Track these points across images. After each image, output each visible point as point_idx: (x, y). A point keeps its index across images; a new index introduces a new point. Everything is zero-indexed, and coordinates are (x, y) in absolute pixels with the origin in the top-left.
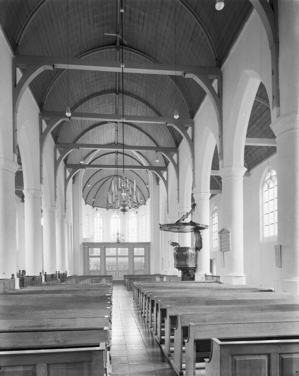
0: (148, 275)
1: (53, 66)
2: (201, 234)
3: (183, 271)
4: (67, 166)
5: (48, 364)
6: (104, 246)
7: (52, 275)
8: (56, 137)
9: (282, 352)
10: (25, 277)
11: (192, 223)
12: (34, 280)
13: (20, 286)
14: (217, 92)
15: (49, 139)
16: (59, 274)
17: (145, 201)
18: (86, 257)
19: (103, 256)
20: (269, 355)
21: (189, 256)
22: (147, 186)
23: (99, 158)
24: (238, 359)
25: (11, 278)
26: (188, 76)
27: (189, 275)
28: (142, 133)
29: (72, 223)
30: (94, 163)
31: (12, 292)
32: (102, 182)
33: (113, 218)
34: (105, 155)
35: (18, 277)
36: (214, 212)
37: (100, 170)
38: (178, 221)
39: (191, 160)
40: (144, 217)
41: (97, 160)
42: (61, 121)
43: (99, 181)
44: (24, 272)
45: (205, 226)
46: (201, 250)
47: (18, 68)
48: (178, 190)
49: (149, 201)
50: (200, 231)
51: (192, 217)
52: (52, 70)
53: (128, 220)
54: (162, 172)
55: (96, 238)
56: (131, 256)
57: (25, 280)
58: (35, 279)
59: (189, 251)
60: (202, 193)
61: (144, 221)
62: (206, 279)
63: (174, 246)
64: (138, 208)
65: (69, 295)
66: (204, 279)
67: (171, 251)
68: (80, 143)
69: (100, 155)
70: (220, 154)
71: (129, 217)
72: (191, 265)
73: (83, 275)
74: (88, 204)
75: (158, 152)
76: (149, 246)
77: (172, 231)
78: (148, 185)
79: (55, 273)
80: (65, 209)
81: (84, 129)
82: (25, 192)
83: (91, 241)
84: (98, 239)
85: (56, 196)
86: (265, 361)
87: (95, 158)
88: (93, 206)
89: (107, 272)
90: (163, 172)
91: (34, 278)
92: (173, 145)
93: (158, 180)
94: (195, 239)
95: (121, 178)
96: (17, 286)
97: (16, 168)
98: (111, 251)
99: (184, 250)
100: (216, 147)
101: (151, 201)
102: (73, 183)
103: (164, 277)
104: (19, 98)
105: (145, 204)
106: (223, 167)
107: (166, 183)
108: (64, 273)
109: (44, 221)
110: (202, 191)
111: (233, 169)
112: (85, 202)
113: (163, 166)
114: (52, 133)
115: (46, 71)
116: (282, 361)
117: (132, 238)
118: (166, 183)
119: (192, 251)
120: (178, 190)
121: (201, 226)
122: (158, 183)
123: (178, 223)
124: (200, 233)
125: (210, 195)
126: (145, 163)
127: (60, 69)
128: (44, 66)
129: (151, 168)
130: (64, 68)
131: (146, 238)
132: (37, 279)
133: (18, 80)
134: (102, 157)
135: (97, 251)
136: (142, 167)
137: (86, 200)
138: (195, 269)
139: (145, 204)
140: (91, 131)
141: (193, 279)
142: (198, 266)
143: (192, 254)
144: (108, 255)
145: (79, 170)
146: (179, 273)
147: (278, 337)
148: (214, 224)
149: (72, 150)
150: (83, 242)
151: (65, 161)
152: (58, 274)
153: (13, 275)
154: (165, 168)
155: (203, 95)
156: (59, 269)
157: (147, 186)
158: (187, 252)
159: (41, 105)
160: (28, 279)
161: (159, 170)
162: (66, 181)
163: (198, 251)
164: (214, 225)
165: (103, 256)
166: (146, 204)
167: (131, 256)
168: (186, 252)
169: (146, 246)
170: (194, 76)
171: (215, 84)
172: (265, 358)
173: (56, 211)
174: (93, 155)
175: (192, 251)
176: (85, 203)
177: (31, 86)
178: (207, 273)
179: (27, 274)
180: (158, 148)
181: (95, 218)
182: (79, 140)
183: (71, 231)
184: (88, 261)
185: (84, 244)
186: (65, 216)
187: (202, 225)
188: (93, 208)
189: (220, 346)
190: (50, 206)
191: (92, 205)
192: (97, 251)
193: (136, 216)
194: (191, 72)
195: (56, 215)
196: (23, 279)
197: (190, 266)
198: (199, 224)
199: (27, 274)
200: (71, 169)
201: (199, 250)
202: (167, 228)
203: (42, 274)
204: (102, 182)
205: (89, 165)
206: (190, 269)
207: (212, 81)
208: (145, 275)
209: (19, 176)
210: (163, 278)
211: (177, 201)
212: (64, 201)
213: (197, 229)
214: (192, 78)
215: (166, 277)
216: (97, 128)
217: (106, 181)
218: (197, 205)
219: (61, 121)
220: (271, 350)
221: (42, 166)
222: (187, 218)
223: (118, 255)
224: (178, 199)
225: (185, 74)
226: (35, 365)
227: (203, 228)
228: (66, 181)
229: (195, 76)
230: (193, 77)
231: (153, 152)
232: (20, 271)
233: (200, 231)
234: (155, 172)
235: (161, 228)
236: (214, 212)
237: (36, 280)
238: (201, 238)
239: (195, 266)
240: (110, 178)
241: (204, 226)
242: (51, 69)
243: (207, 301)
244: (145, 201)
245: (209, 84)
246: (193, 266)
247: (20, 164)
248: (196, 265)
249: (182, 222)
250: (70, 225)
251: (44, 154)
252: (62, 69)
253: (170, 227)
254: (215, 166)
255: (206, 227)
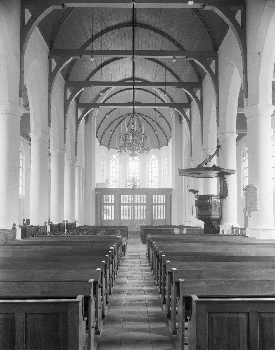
0: (170, 226)
1: (63, 5)
2: (226, 180)
3: (206, 223)
4: (79, 105)
5: (26, 314)
6: (118, 193)
7: (59, 225)
8: (66, 76)
9: (262, 310)
10: (29, 227)
11: (215, 168)
12: (38, 231)
13: (22, 237)
14: (240, 24)
15: (59, 78)
16: (67, 224)
17: (167, 141)
18: (99, 205)
19: (118, 204)
20: (248, 314)
21: (213, 205)
22: (156, 133)
23: (115, 95)
24: (214, 316)
25: (12, 228)
26: (207, 8)
27: (212, 227)
28: (162, 67)
29: (84, 167)
30: (109, 101)
31: (13, 243)
32: (119, 120)
33: (130, 160)
34: (122, 92)
35: (20, 226)
36: (245, 153)
37: (115, 108)
38: (200, 165)
39: (215, 97)
40: (166, 159)
41: (112, 97)
42: (71, 59)
43: (110, 125)
44: (28, 221)
45: (231, 170)
46: (226, 198)
47: (26, 8)
48: (202, 129)
49: (171, 141)
50: (225, 176)
51: (218, 161)
52: (61, 9)
53: (148, 162)
54: (184, 109)
55: (111, 184)
56: (150, 204)
57: (28, 231)
58: (40, 229)
59: (213, 199)
60: (227, 134)
61: (166, 163)
62: (232, 232)
63: (195, 194)
64: (160, 149)
65: (70, 248)
66: (231, 232)
67: (192, 199)
68: (94, 81)
69: (116, 92)
70: (244, 91)
71: (149, 160)
72: (215, 215)
73: (94, 225)
74: (103, 145)
75: (178, 88)
76: (171, 193)
77: (193, 176)
78: (156, 132)
79: (62, 223)
80: (76, 151)
81: (98, 65)
82: (32, 135)
83: (106, 187)
84: (113, 185)
85: (65, 139)
86: (244, 320)
87: (109, 96)
88: (108, 147)
89: (122, 222)
90: (186, 110)
91: (38, 228)
92: (196, 80)
93: (181, 118)
94: (220, 185)
95: (140, 116)
96: (19, 237)
97: (23, 111)
98: (127, 198)
99: (207, 198)
100: (241, 85)
101: (173, 140)
102: (86, 123)
103: (184, 229)
104: (29, 32)
105: (167, 145)
106: (247, 105)
107: (189, 122)
108: (72, 223)
109: (53, 166)
110: (227, 132)
111: (259, 108)
112: (100, 143)
113: (186, 103)
114: (62, 72)
115: (55, 11)
116: (262, 320)
117: (153, 184)
118: (189, 122)
119: (216, 200)
120: (202, 129)
121: (225, 171)
122: (181, 122)
123: (199, 168)
124: (225, 178)
125: (236, 136)
126: (167, 101)
127: (70, 8)
128: (53, 6)
129: (172, 105)
130: (73, 7)
131: (168, 184)
132: (41, 229)
133: (26, 21)
134: (119, 94)
135: (111, 198)
136: (164, 104)
137: (101, 141)
138: (219, 221)
139: (167, 145)
140: (105, 67)
141: (218, 231)
142: (224, 216)
143: (216, 203)
144: (123, 203)
145: (92, 109)
146: (201, 224)
147: (253, 297)
148: (245, 168)
149: (83, 89)
150: (96, 188)
151: (77, 100)
152: (65, 224)
153: (14, 225)
154: (188, 105)
155: (225, 28)
156: (67, 218)
157: (156, 133)
158: (210, 201)
159: (51, 43)
160: (32, 229)
161: (182, 107)
162: (78, 122)
163: (223, 199)
164: (245, 169)
165: (118, 204)
166: (169, 144)
167: (150, 204)
168: (209, 201)
169: (167, 193)
170: (213, 8)
171: (238, 17)
172: (243, 317)
173: (65, 155)
174: (107, 93)
175: (216, 200)
176: (100, 144)
177: (40, 26)
178: (233, 225)
179: (32, 223)
180: (179, 84)
181: (111, 161)
182: (93, 77)
183: (82, 176)
184: (101, 208)
185: (97, 190)
186: (76, 160)
187: (227, 170)
188: (108, 149)
189: (195, 303)
190: (59, 149)
191: (107, 145)
192: (111, 198)
193: (157, 158)
194: (210, 4)
195: (65, 158)
196: (27, 230)
197: (213, 217)
198: (224, 169)
199: (32, 223)
200: (83, 109)
201: (224, 199)
202: (187, 173)
203: (47, 224)
204: (119, 120)
205: (104, 104)
206: (214, 219)
207: (235, 13)
208: (165, 226)
209: (25, 119)
210: (183, 230)
211: (200, 142)
212: (75, 143)
213: (222, 174)
214: (212, 10)
215: (186, 229)
216: (111, 64)
217: (123, 119)
218: (221, 147)
219: (71, 59)
220: (249, 309)
221: (51, 107)
222: (209, 161)
223: (135, 203)
224: (202, 140)
225: (204, 6)
226: (14, 314)
227: (229, 174)
228: (78, 122)
229: (215, 8)
230: (213, 9)
231: (174, 88)
232: (24, 220)
233: (225, 176)
234: (176, 109)
235: (180, 173)
236: (245, 153)
237: (41, 230)
238: (226, 185)
239: (219, 217)
240: (128, 116)
241: (229, 171)
242: (61, 9)
243: (216, 257)
244: (167, 141)
245: (231, 16)
246: (218, 217)
247: (27, 106)
248: (221, 216)
249: (204, 166)
250: (82, 169)
251: (52, 95)
252: (71, 7)
253: (190, 172)
254: (241, 105)
255: (232, 172)
